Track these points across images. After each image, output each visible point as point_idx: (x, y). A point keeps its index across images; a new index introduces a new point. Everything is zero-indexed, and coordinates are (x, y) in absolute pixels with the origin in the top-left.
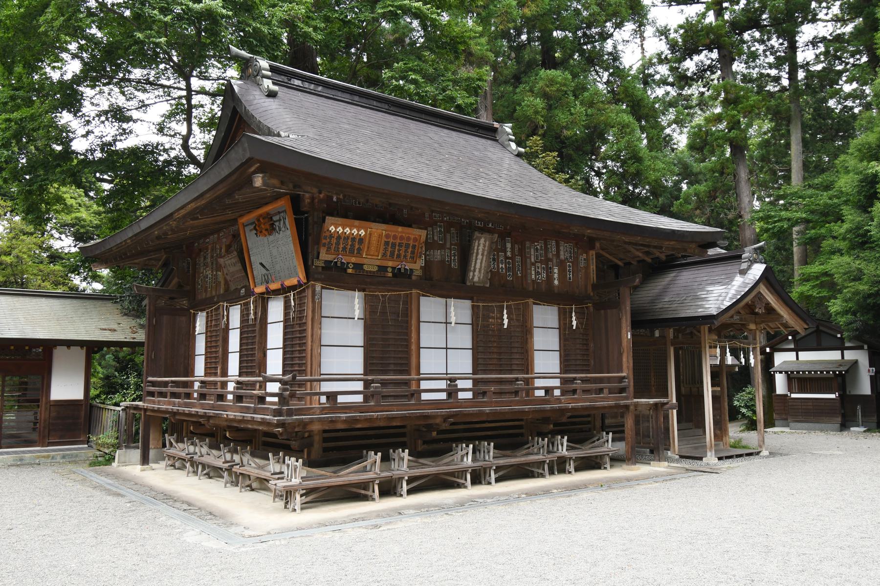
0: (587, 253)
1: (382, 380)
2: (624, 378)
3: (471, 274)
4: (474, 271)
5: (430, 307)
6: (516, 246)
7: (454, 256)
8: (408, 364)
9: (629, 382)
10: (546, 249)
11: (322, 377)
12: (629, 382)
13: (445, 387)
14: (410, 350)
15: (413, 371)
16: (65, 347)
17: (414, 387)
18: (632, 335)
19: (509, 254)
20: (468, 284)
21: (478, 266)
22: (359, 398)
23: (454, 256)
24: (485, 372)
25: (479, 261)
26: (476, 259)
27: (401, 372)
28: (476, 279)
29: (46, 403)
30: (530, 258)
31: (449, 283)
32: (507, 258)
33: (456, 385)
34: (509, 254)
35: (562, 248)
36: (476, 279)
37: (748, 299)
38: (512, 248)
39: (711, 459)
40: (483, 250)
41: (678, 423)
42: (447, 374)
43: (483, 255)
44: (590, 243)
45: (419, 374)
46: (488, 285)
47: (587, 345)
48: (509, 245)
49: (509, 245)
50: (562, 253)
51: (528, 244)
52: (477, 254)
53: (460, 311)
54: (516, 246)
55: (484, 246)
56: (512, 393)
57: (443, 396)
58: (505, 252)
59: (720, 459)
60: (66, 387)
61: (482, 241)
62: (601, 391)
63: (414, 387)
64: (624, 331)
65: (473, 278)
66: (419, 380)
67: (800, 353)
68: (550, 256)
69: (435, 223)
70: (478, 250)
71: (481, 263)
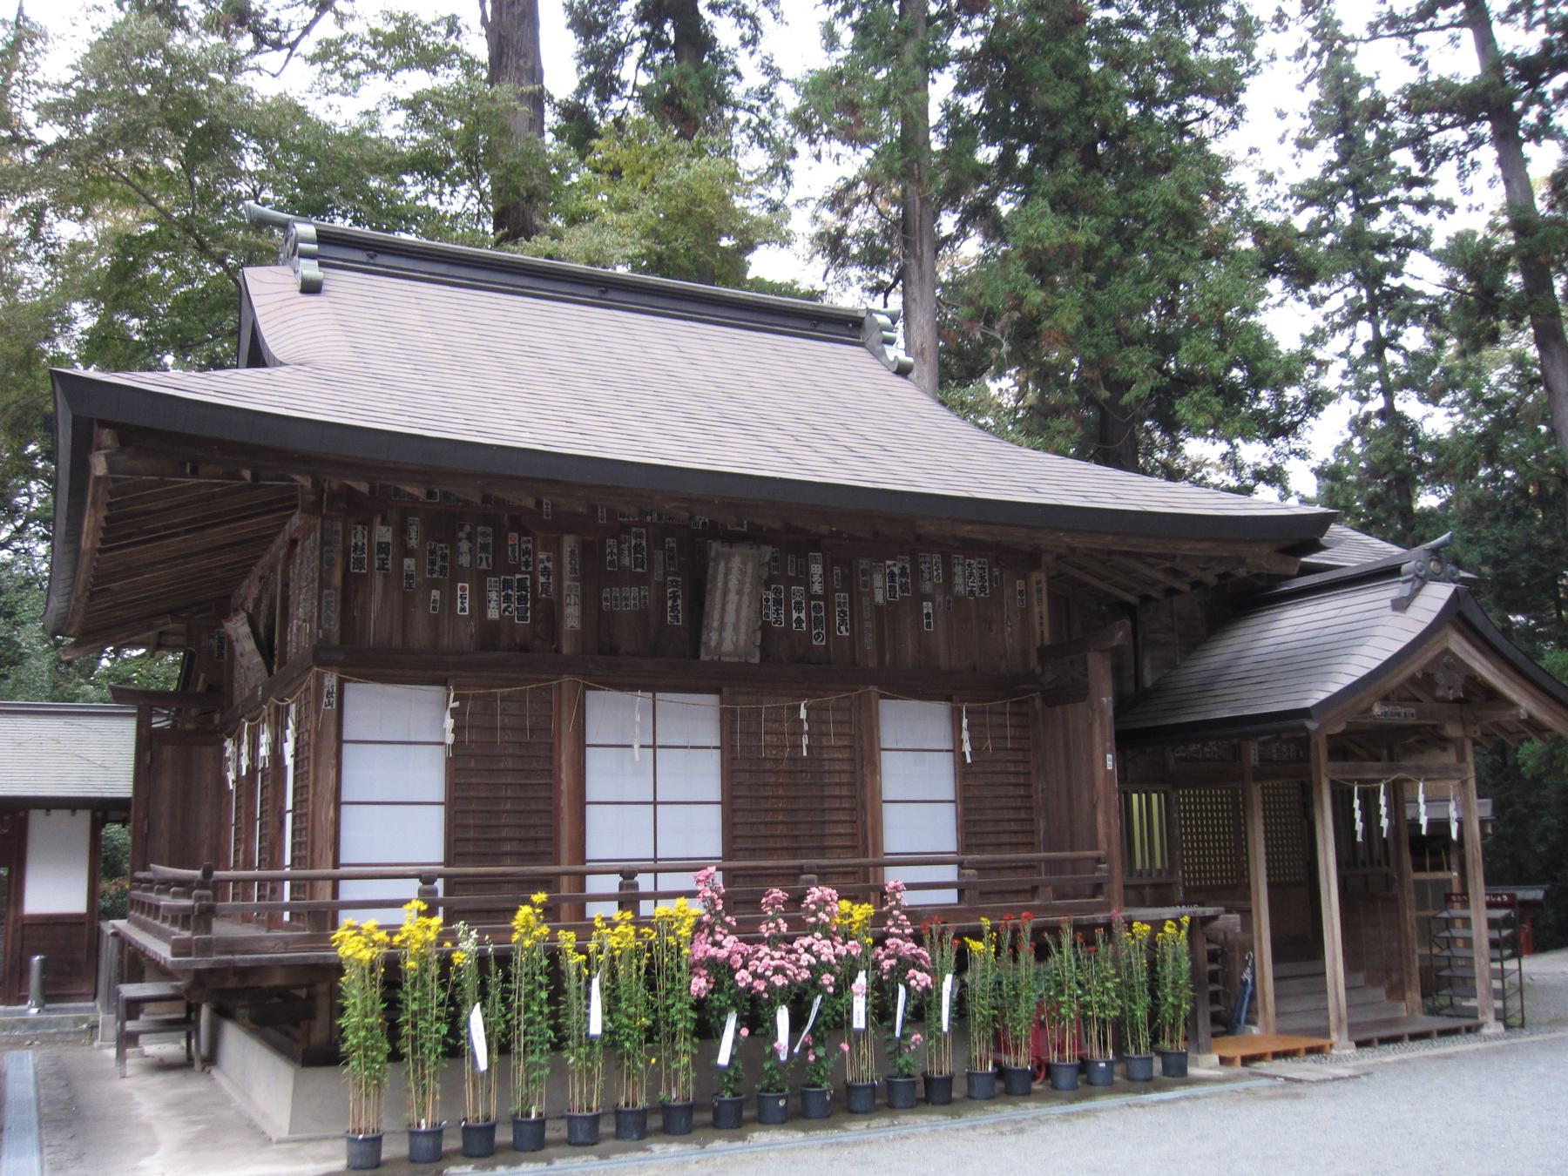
0: (1025, 577)
1: (978, 862)
2: (1098, 860)
3: (714, 636)
4: (722, 629)
5: (611, 716)
6: (837, 570)
7: (675, 598)
8: (553, 840)
9: (1110, 871)
10: (917, 574)
11: (343, 870)
12: (1110, 871)
13: (616, 890)
14: (558, 808)
15: (565, 854)
16: (67, 812)
17: (324, 895)
18: (1117, 760)
19: (817, 588)
20: (704, 657)
21: (730, 617)
22: (950, 896)
23: (675, 598)
24: (752, 853)
25: (731, 608)
26: (724, 604)
27: (535, 858)
28: (728, 646)
29: (16, 920)
30: (871, 594)
31: (663, 658)
32: (811, 597)
33: (636, 886)
34: (817, 588)
35: (958, 570)
36: (728, 646)
37: (1414, 667)
38: (826, 575)
39: (1342, 1045)
40: (741, 582)
41: (1274, 962)
42: (655, 859)
43: (740, 593)
44: (1029, 560)
45: (336, 865)
46: (756, 660)
47: (1027, 785)
48: (817, 570)
49: (817, 570)
50: (958, 580)
51: (864, 563)
52: (726, 591)
53: (694, 720)
54: (837, 570)
55: (743, 573)
56: (1025, 891)
57: (950, 896)
58: (807, 584)
59: (1360, 1044)
60: (54, 890)
61: (736, 562)
62: (1033, 891)
63: (324, 895)
64: (1098, 751)
65: (719, 644)
66: (336, 881)
67: (885, 797)
68: (927, 587)
69: (625, 528)
70: (726, 583)
71: (738, 611)
